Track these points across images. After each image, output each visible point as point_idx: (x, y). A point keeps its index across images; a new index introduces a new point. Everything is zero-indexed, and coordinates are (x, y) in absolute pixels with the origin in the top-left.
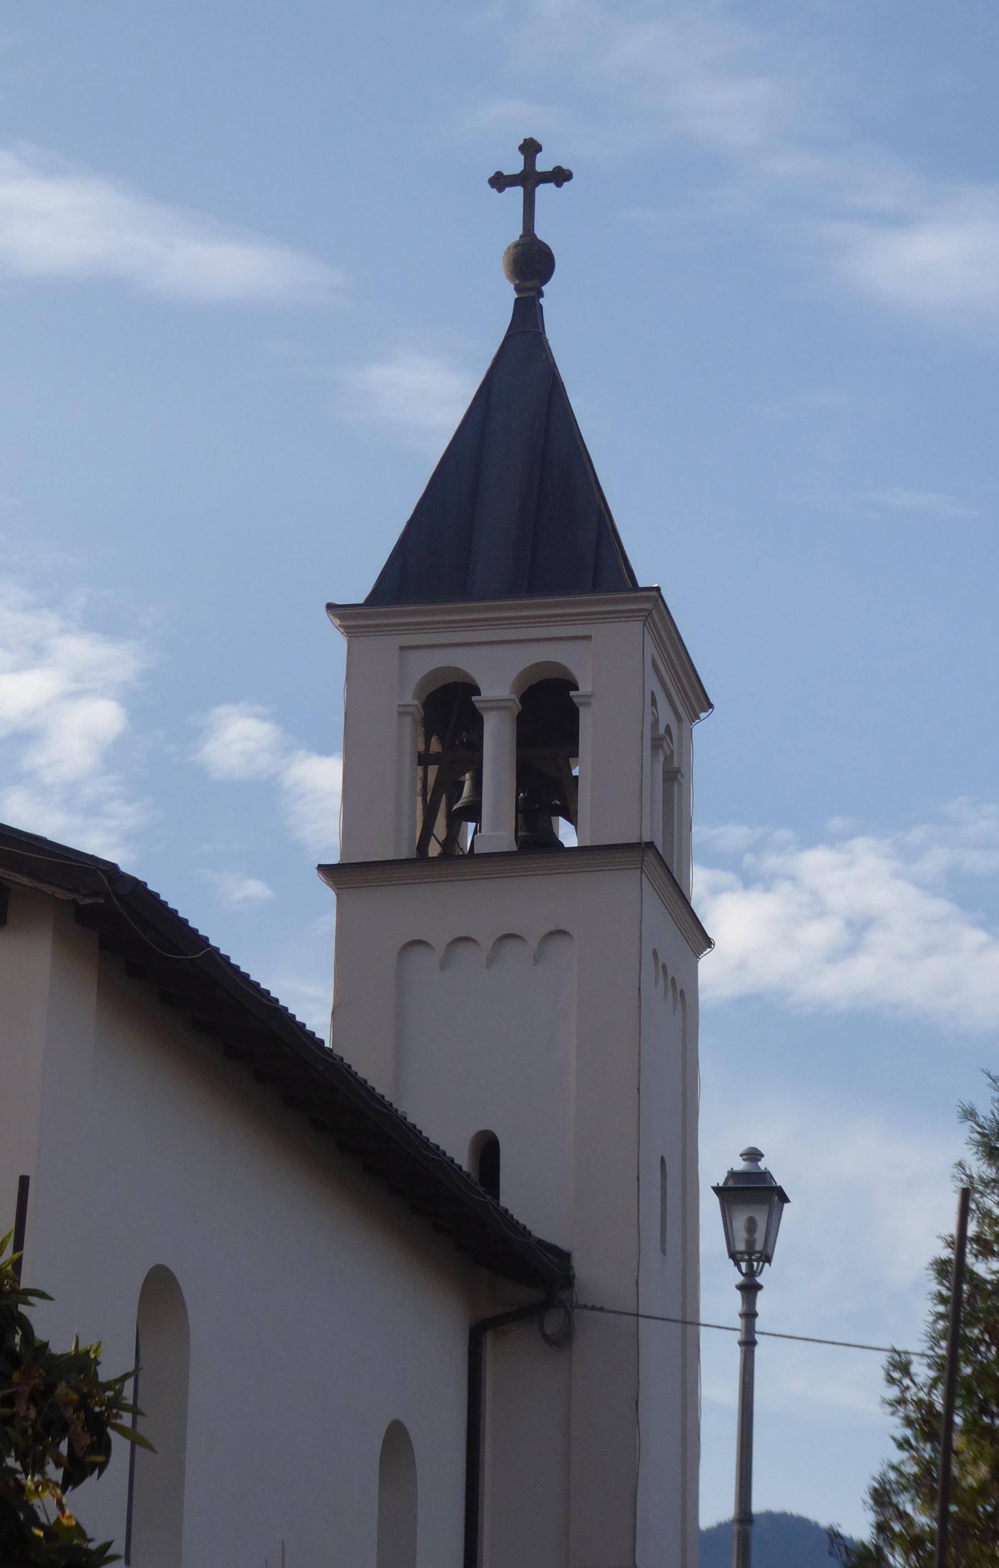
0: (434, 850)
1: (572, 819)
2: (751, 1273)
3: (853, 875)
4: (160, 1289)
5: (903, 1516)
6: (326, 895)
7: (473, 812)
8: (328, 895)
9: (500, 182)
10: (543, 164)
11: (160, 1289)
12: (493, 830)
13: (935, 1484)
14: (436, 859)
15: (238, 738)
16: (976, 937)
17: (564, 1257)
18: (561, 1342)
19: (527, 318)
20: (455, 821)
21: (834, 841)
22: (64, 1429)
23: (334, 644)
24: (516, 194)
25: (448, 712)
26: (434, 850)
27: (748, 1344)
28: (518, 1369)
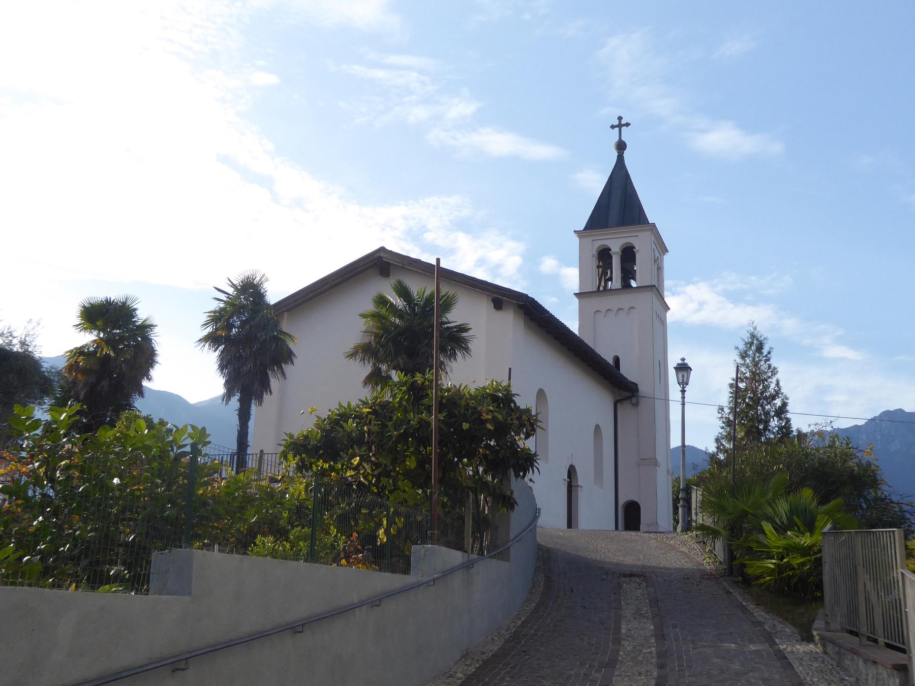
0: (601, 289)
1: (635, 280)
2: (683, 388)
3: (700, 291)
4: (541, 394)
5: (723, 445)
6: (576, 300)
7: (611, 279)
8: (576, 300)
9: (613, 127)
10: (623, 122)
11: (541, 394)
12: (616, 282)
13: (731, 437)
14: (602, 291)
15: (549, 264)
16: (731, 306)
17: (636, 385)
18: (636, 405)
19: (620, 159)
20: (606, 281)
21: (694, 283)
22: (525, 426)
23: (576, 240)
24: (617, 129)
25: (604, 255)
26: (601, 289)
27: (683, 404)
28: (625, 411)
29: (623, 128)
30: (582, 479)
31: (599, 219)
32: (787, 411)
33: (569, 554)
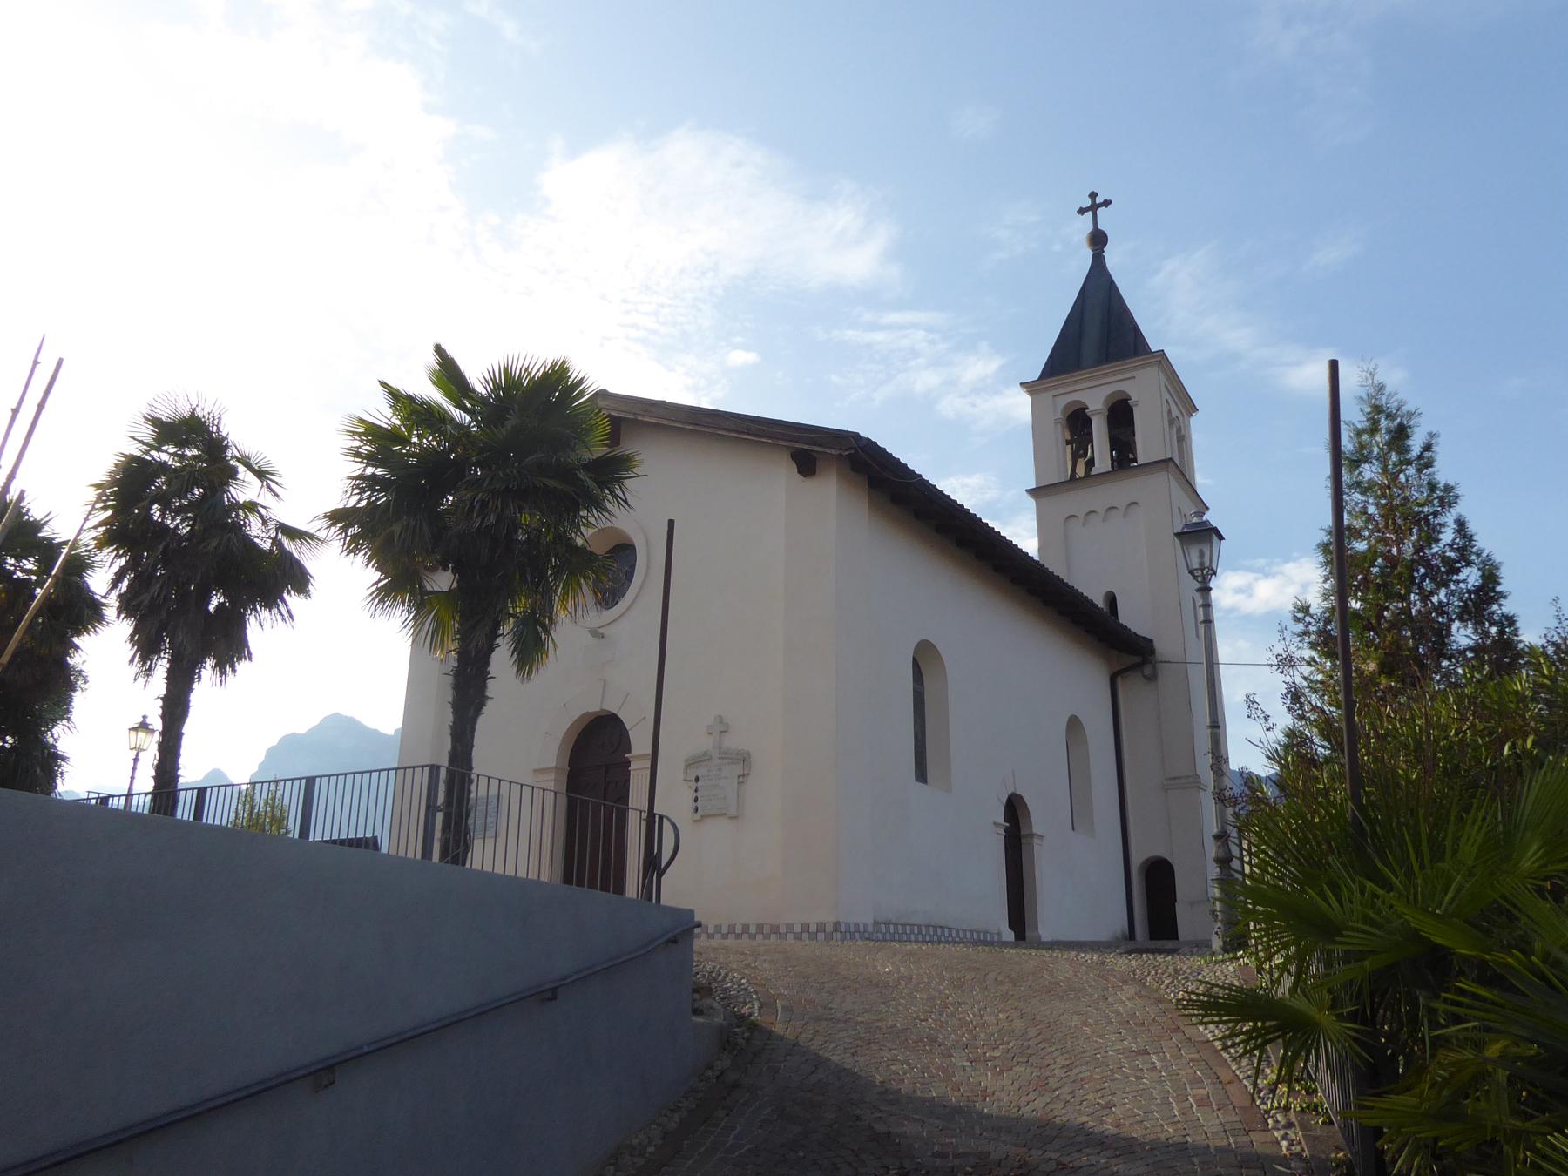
9: (1082, 211)
10: (1099, 200)
12: (1103, 463)
18: (1152, 678)
19: (1098, 263)
21: (1295, 560)
25: (1078, 422)
29: (1100, 211)
30: (1043, 819)
31: (1067, 358)
32: (1502, 595)
33: (819, 1062)
